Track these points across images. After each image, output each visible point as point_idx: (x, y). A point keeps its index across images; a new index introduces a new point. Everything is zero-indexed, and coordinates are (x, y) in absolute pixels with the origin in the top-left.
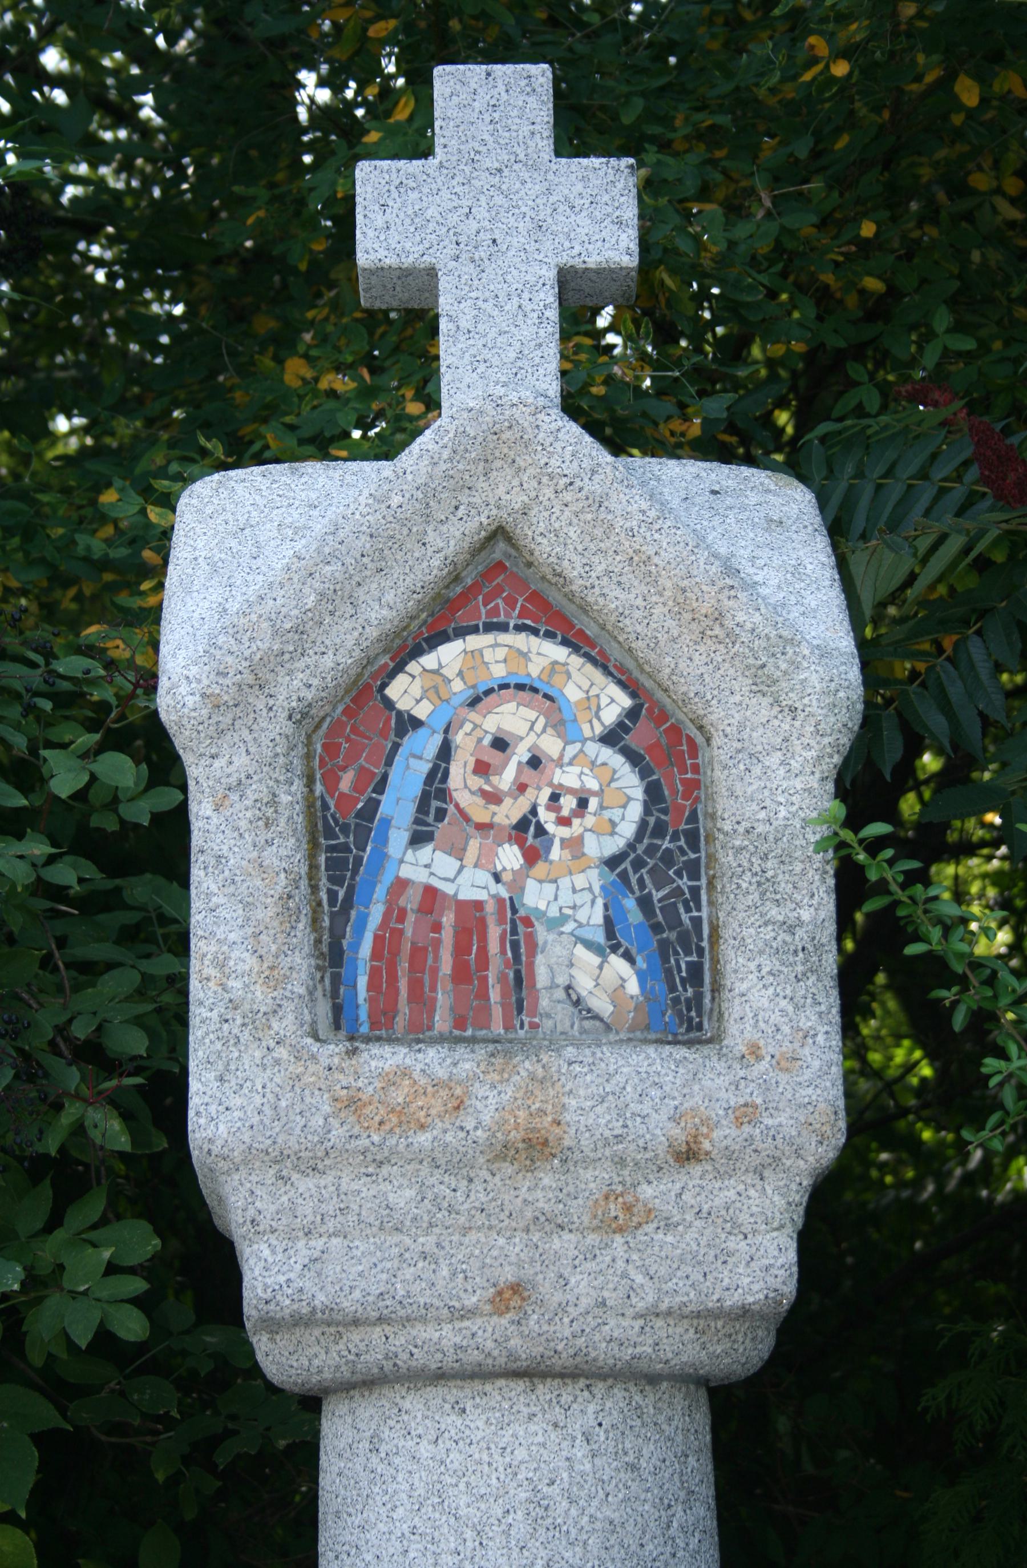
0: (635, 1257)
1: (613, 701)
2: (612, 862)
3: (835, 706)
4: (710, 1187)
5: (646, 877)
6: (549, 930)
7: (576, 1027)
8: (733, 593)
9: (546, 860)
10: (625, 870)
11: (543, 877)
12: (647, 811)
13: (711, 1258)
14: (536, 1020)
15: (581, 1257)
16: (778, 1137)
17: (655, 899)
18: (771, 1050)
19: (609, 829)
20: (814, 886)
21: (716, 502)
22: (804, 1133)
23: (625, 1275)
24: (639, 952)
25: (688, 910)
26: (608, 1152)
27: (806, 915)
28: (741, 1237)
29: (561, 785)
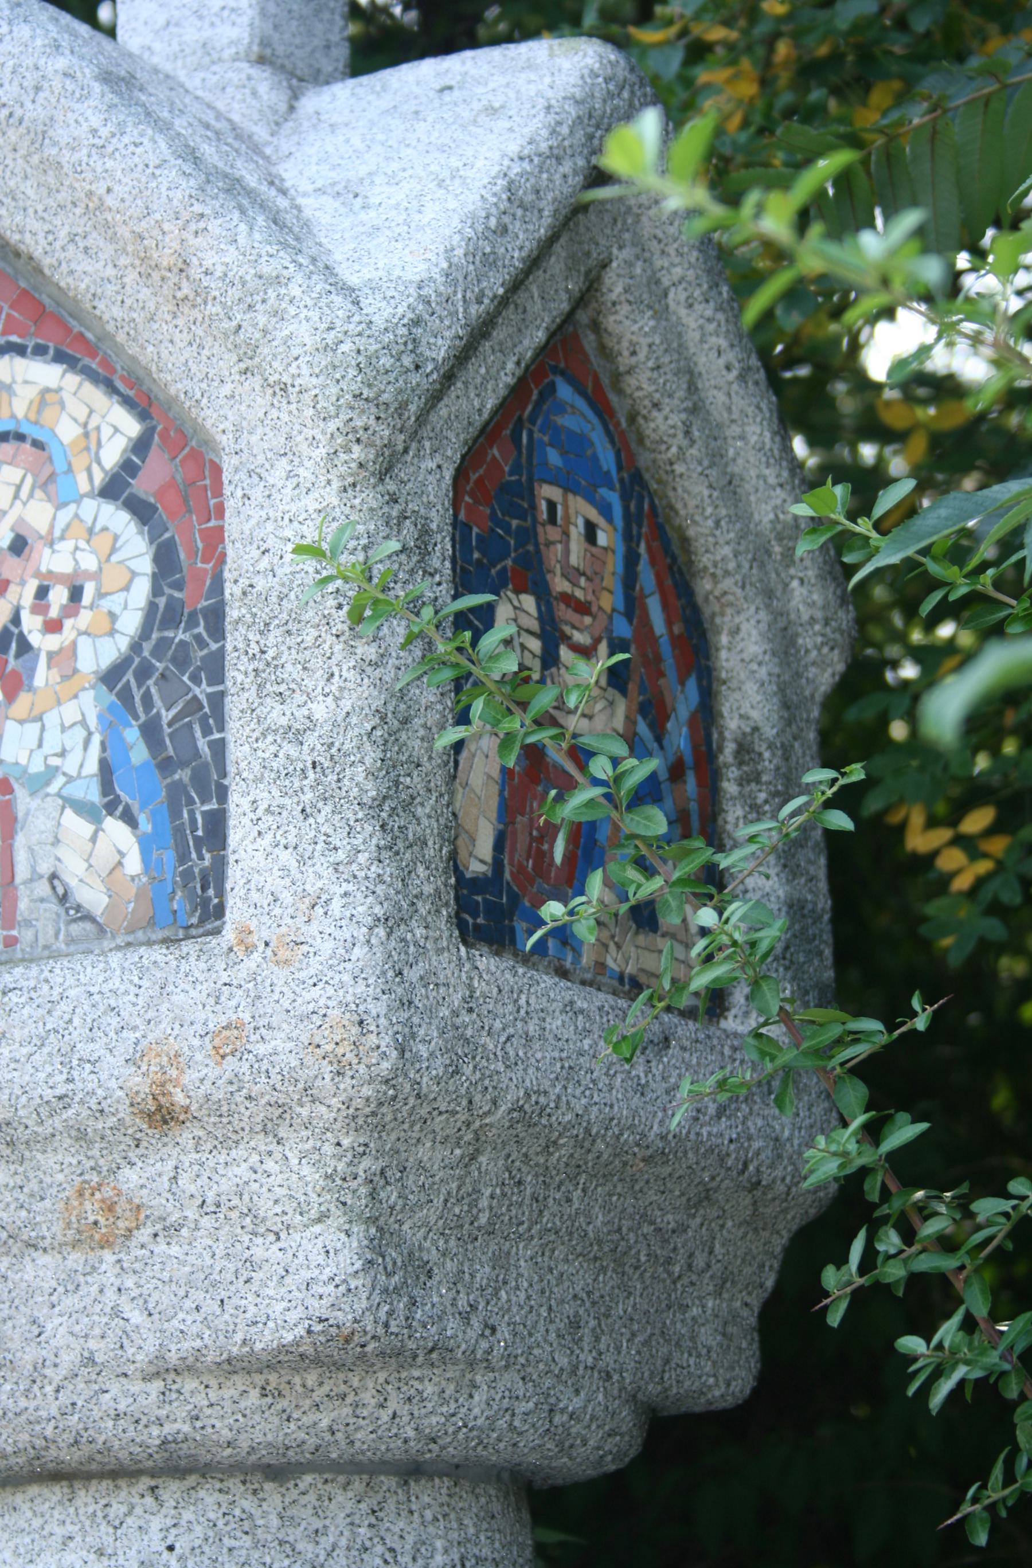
0: (129, 1283)
1: (116, 430)
2: (111, 677)
3: (335, 367)
4: (211, 1163)
5: (153, 690)
6: (33, 794)
7: (62, 937)
8: (202, 225)
9: (30, 689)
10: (127, 685)
11: (24, 716)
12: (156, 590)
13: (230, 1276)
14: (15, 933)
15: (61, 1289)
16: (273, 1072)
17: (165, 721)
18: (265, 935)
19: (106, 626)
20: (334, 661)
21: (447, 97)
22: (309, 1060)
23: (116, 1312)
24: (142, 809)
25: (207, 731)
26: (57, 1122)
27: (320, 710)
28: (272, 1237)
29: (50, 573)
